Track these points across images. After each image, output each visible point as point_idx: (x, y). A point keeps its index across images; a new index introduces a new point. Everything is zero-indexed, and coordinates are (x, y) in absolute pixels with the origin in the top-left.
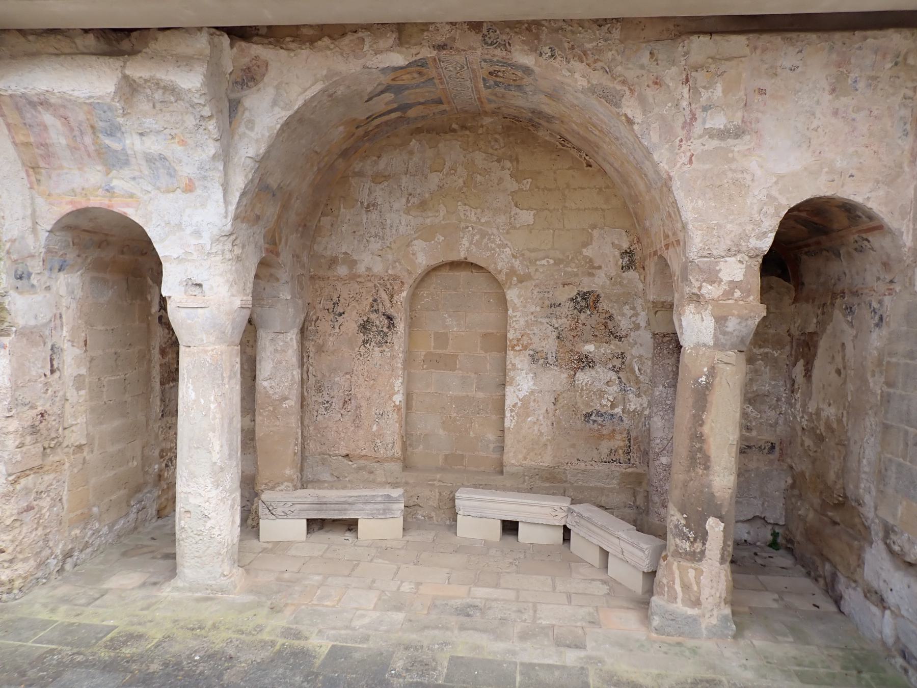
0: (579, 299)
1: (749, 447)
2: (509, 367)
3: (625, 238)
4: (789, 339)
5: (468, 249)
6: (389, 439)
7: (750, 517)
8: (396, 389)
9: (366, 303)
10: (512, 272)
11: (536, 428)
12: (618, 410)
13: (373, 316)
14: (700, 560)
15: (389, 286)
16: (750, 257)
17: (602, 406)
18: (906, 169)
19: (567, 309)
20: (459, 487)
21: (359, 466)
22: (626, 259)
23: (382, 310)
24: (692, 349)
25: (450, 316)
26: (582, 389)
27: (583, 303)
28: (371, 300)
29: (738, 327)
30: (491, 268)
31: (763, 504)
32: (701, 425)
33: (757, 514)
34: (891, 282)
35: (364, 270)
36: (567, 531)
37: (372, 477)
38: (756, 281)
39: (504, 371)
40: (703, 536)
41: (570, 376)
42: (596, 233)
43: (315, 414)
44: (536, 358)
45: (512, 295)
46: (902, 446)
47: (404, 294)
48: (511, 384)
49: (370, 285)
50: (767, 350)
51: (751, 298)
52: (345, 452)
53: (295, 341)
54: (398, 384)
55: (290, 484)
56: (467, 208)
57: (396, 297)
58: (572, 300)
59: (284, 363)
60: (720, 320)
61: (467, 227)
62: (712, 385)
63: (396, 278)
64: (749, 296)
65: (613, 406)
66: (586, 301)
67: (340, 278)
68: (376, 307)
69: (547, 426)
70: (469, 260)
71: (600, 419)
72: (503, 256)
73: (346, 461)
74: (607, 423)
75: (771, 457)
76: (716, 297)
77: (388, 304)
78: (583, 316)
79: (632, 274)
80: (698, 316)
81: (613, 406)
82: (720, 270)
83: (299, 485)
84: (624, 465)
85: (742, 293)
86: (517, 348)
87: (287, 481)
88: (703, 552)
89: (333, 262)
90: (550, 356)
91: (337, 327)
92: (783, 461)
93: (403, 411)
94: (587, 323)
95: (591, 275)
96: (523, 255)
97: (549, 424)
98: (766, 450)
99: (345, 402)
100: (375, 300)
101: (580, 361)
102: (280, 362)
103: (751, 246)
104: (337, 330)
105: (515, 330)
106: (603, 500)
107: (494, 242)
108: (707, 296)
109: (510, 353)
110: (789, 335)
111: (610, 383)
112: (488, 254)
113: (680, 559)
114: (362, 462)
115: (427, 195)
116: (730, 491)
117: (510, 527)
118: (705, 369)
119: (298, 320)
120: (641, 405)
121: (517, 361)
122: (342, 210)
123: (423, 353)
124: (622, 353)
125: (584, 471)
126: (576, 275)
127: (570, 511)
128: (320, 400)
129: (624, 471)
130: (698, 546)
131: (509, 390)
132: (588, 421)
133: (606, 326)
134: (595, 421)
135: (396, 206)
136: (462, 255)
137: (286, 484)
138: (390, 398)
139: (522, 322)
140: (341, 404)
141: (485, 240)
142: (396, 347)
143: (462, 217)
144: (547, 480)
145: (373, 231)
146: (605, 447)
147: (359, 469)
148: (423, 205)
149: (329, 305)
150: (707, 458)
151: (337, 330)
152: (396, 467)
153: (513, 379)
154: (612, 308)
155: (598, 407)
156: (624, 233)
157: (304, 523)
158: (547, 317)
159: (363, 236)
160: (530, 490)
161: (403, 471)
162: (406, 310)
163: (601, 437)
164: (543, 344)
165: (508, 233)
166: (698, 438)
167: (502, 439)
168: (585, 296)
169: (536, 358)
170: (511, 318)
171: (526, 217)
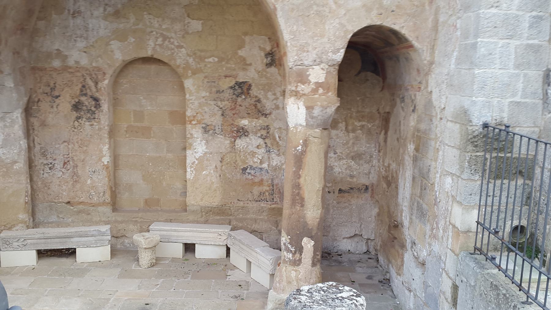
0: (237, 87)
1: (351, 188)
2: (189, 136)
3: (268, 43)
4: (378, 115)
5: (154, 49)
6: (101, 190)
7: (352, 234)
8: (104, 153)
9: (77, 89)
10: (187, 66)
11: (208, 179)
12: (265, 166)
13: (83, 99)
14: (299, 265)
15: (94, 76)
16: (329, 66)
17: (254, 162)
18: (427, 7)
19: (228, 94)
20: (152, 222)
21: (78, 209)
22: (269, 59)
23: (89, 94)
24: (293, 127)
25: (144, 98)
26: (240, 151)
27: (239, 91)
28: (80, 86)
29: (321, 113)
30: (172, 63)
31: (361, 226)
32: (299, 178)
33: (357, 233)
34: (420, 83)
35: (73, 63)
36: (228, 249)
37: (89, 217)
38: (334, 81)
39: (185, 137)
40: (300, 249)
41: (231, 142)
42: (247, 39)
43: (42, 172)
44: (207, 129)
45: (188, 83)
46: (419, 190)
47: (106, 82)
48: (190, 149)
49: (79, 74)
50: (364, 123)
51: (330, 94)
52: (66, 201)
53: (20, 119)
54: (105, 148)
55: (23, 225)
56: (151, 17)
57: (100, 85)
58: (231, 88)
59: (12, 135)
60: (309, 108)
61: (152, 32)
62: (305, 151)
63: (99, 69)
64: (328, 92)
65: (261, 163)
66: (242, 89)
67: (55, 70)
68: (84, 92)
69: (217, 177)
70: (155, 56)
71: (253, 172)
72: (180, 55)
73: (68, 206)
74: (258, 174)
75: (366, 195)
76: (307, 93)
77: (94, 89)
78: (239, 99)
79: (273, 70)
80: (296, 106)
81: (261, 163)
82: (310, 75)
83: (31, 225)
84: (269, 203)
85: (324, 90)
86: (194, 122)
87: (21, 223)
88: (300, 260)
89: (49, 56)
90: (217, 128)
91: (55, 107)
92: (373, 197)
93: (111, 168)
94: (242, 104)
95: (244, 69)
96: (195, 54)
97: (218, 176)
98: (363, 190)
99: (65, 163)
100: (84, 86)
101: (238, 131)
102: (9, 135)
103: (329, 58)
104: (55, 109)
105: (192, 109)
106: (255, 227)
107: (172, 43)
108: (301, 92)
109: (189, 126)
110: (379, 113)
111: (259, 147)
112: (169, 53)
113: (286, 265)
114: (81, 207)
115: (119, 6)
116: (318, 220)
117: (189, 248)
118: (301, 141)
119: (21, 103)
120: (281, 161)
121: (193, 132)
122: (54, 16)
123: (126, 126)
124: (267, 126)
125: (243, 207)
126: (234, 70)
127: (230, 235)
128: (45, 162)
129: (269, 207)
130: (297, 256)
131: (189, 152)
132: (245, 174)
133: (255, 106)
134: (249, 173)
135: (96, 13)
136: (149, 53)
137: (20, 225)
138: (100, 159)
139: (196, 103)
140: (62, 165)
141: (166, 42)
142: (102, 122)
143: (148, 23)
144: (218, 214)
145: (79, 32)
146: (256, 190)
147: (80, 212)
148: (117, 14)
149: (48, 90)
150: (302, 199)
151: (55, 109)
152: (107, 210)
153: (191, 145)
154: (260, 93)
155: (251, 163)
156: (267, 40)
157: (34, 253)
158: (215, 100)
159: (71, 36)
160: (206, 222)
161: (113, 212)
162: (109, 94)
163: (254, 184)
164: (212, 119)
165: (183, 37)
166: (297, 186)
167: (185, 187)
168: (240, 85)
169: (207, 129)
170: (189, 100)
171: (196, 25)
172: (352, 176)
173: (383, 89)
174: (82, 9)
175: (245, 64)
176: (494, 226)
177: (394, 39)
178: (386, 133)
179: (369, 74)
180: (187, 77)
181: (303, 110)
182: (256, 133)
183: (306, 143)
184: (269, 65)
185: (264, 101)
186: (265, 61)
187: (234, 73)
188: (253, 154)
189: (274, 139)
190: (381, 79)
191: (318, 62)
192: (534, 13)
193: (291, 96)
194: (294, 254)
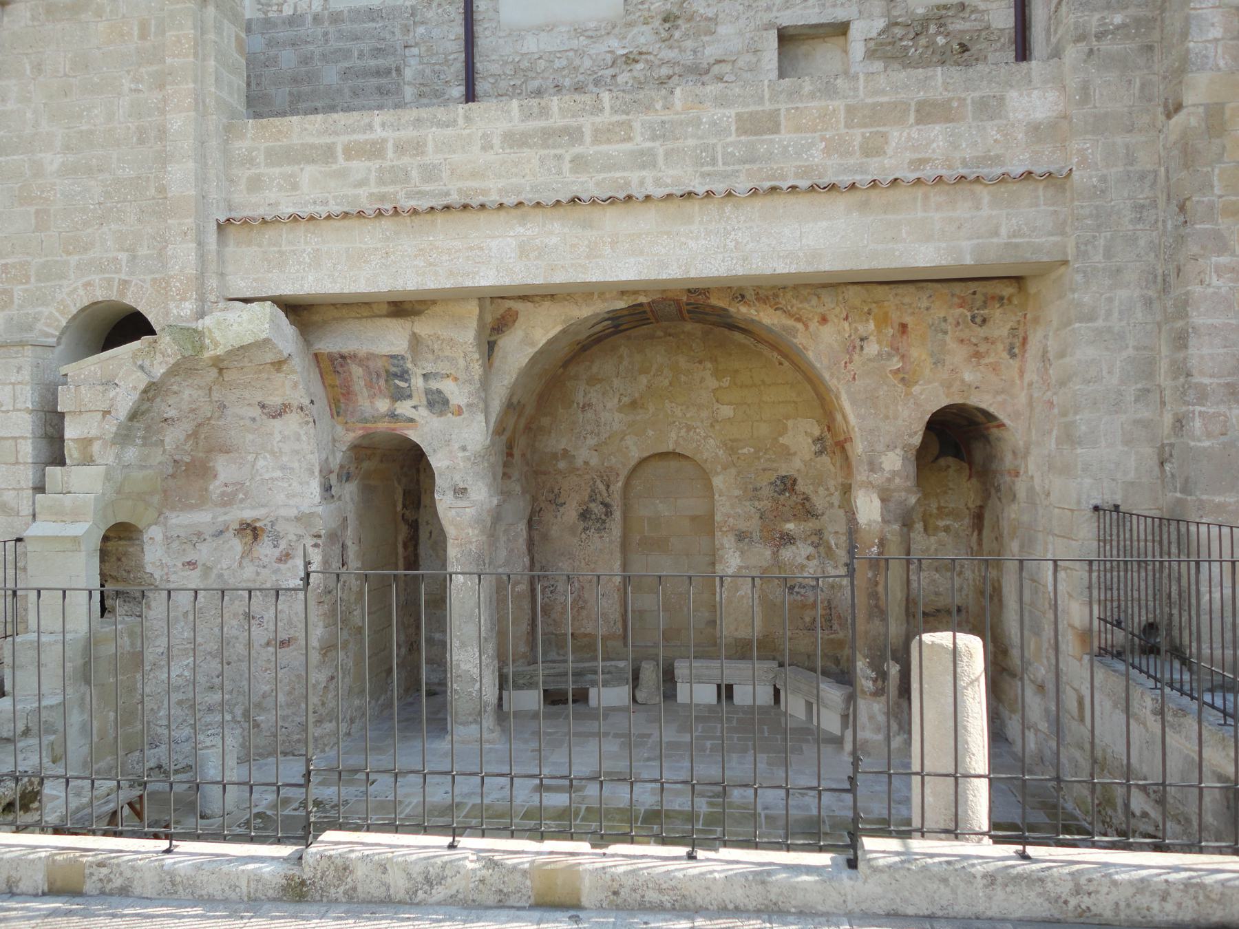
5: (676, 442)
9: (586, 495)
13: (592, 505)
18: (1018, 382)
41: (773, 553)
42: (790, 423)
45: (718, 481)
71: (803, 591)
77: (605, 495)
78: (782, 498)
88: (883, 689)
100: (593, 491)
101: (781, 538)
102: (512, 550)
112: (695, 445)
121: (725, 541)
135: (609, 405)
149: (552, 496)
153: (722, 557)
165: (712, 426)
172: (937, 594)
173: (970, 477)
174: (594, 401)
175: (787, 453)
176: (1116, 617)
177: (981, 418)
178: (980, 533)
179: (950, 460)
180: (717, 474)
181: (877, 503)
182: (806, 540)
183: (882, 544)
184: (819, 453)
185: (814, 499)
186: (813, 448)
187: (775, 465)
188: (803, 567)
189: (830, 548)
190: (965, 465)
191: (890, 447)
192: (1139, 386)
193: (860, 487)
194: (875, 681)
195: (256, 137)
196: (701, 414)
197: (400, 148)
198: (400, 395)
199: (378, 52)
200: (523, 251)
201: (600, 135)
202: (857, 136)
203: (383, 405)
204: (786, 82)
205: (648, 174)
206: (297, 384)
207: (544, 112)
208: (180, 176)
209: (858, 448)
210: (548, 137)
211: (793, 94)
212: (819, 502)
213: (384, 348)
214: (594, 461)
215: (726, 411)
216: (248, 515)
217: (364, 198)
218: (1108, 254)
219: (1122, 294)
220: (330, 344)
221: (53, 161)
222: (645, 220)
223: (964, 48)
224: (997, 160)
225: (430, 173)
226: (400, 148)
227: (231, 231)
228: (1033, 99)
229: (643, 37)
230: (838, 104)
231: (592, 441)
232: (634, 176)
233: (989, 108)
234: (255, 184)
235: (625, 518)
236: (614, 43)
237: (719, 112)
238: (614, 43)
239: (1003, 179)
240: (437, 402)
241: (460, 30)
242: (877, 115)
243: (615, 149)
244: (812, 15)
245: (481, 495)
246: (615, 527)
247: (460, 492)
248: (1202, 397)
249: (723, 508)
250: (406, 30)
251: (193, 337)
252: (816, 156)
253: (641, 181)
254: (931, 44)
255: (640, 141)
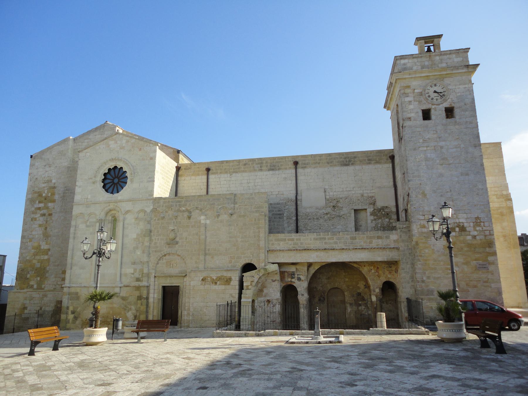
45: (346, 293)
175: (359, 288)
184: (365, 288)
195: (272, 237)
196: (342, 281)
197: (297, 240)
198: (293, 278)
199: (279, 211)
200: (317, 256)
201: (329, 239)
202: (368, 240)
203: (289, 280)
204: (357, 232)
205: (336, 245)
206: (278, 277)
207: (320, 235)
208: (262, 243)
209: (372, 288)
210: (321, 239)
211: (358, 234)
212: (366, 298)
213: (292, 270)
214: (321, 289)
215: (347, 280)
216: (268, 298)
217: (291, 247)
218: (406, 260)
219: (408, 266)
220: (283, 270)
221: (239, 240)
222: (336, 252)
223: (388, 214)
224: (389, 245)
225: (302, 244)
226: (297, 240)
227: (269, 252)
228: (394, 236)
229: (329, 210)
230: (365, 236)
231: (321, 285)
232: (334, 245)
233: (388, 237)
234: (273, 244)
235: (327, 301)
236: (324, 211)
237: (347, 236)
238: (324, 211)
239: (390, 248)
240: (299, 279)
241: (295, 207)
242: (371, 238)
243: (331, 241)
244: (360, 208)
245: (306, 296)
246: (326, 302)
247: (303, 295)
248: (418, 282)
249: (347, 299)
250: (284, 207)
251: (265, 269)
252: (362, 243)
253: (336, 246)
254: (382, 213)
255: (335, 240)
